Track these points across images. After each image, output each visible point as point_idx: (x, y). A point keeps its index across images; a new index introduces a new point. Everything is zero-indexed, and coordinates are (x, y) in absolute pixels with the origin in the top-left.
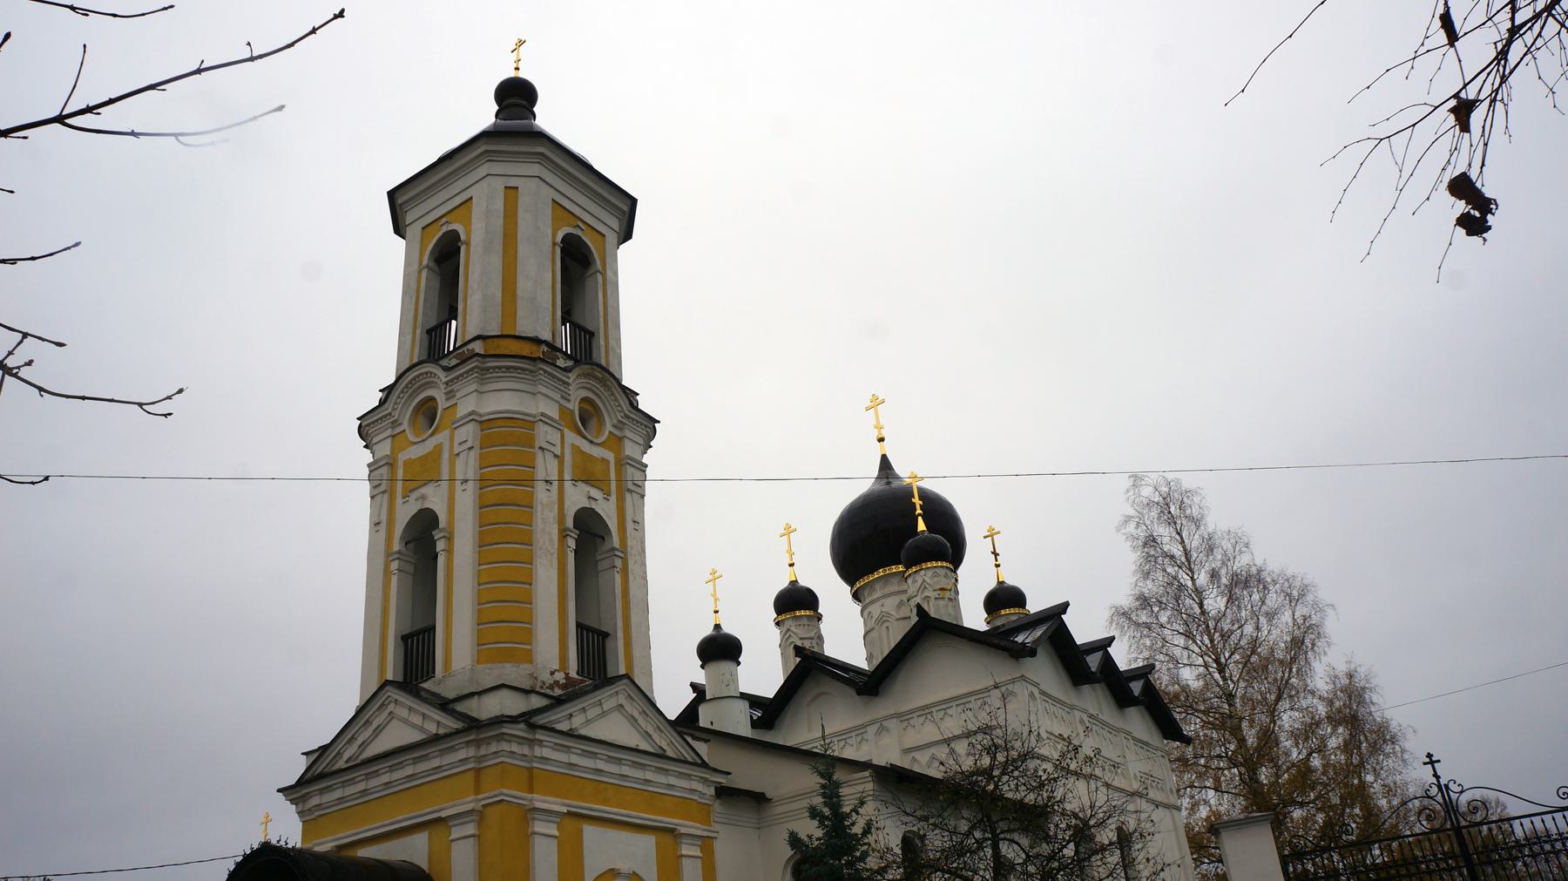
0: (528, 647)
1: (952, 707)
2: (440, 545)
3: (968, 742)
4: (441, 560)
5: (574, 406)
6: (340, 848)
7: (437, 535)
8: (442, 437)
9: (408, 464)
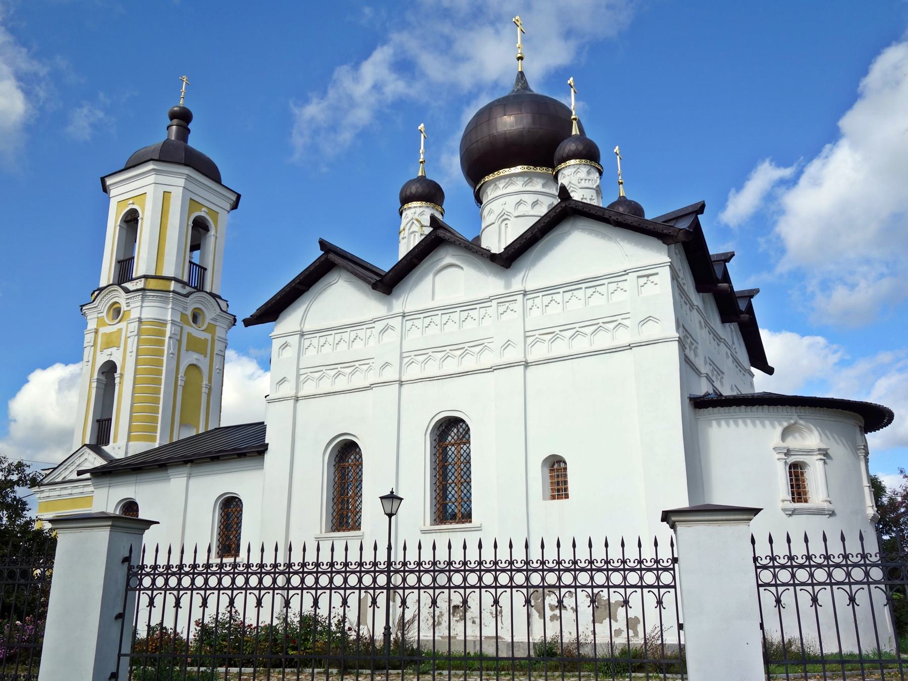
0: (156, 425)
1: (581, 288)
2: (117, 381)
3: (647, 279)
4: (117, 388)
5: (189, 313)
6: (63, 479)
7: (116, 375)
8: (123, 325)
9: (105, 334)
